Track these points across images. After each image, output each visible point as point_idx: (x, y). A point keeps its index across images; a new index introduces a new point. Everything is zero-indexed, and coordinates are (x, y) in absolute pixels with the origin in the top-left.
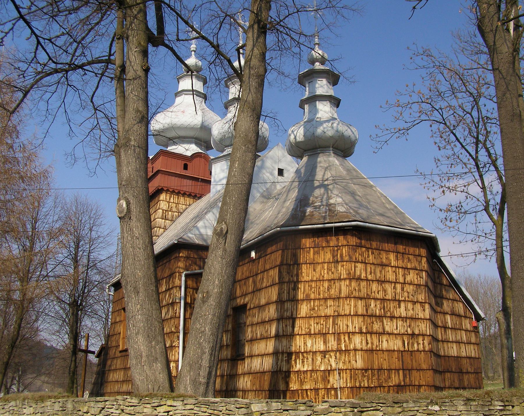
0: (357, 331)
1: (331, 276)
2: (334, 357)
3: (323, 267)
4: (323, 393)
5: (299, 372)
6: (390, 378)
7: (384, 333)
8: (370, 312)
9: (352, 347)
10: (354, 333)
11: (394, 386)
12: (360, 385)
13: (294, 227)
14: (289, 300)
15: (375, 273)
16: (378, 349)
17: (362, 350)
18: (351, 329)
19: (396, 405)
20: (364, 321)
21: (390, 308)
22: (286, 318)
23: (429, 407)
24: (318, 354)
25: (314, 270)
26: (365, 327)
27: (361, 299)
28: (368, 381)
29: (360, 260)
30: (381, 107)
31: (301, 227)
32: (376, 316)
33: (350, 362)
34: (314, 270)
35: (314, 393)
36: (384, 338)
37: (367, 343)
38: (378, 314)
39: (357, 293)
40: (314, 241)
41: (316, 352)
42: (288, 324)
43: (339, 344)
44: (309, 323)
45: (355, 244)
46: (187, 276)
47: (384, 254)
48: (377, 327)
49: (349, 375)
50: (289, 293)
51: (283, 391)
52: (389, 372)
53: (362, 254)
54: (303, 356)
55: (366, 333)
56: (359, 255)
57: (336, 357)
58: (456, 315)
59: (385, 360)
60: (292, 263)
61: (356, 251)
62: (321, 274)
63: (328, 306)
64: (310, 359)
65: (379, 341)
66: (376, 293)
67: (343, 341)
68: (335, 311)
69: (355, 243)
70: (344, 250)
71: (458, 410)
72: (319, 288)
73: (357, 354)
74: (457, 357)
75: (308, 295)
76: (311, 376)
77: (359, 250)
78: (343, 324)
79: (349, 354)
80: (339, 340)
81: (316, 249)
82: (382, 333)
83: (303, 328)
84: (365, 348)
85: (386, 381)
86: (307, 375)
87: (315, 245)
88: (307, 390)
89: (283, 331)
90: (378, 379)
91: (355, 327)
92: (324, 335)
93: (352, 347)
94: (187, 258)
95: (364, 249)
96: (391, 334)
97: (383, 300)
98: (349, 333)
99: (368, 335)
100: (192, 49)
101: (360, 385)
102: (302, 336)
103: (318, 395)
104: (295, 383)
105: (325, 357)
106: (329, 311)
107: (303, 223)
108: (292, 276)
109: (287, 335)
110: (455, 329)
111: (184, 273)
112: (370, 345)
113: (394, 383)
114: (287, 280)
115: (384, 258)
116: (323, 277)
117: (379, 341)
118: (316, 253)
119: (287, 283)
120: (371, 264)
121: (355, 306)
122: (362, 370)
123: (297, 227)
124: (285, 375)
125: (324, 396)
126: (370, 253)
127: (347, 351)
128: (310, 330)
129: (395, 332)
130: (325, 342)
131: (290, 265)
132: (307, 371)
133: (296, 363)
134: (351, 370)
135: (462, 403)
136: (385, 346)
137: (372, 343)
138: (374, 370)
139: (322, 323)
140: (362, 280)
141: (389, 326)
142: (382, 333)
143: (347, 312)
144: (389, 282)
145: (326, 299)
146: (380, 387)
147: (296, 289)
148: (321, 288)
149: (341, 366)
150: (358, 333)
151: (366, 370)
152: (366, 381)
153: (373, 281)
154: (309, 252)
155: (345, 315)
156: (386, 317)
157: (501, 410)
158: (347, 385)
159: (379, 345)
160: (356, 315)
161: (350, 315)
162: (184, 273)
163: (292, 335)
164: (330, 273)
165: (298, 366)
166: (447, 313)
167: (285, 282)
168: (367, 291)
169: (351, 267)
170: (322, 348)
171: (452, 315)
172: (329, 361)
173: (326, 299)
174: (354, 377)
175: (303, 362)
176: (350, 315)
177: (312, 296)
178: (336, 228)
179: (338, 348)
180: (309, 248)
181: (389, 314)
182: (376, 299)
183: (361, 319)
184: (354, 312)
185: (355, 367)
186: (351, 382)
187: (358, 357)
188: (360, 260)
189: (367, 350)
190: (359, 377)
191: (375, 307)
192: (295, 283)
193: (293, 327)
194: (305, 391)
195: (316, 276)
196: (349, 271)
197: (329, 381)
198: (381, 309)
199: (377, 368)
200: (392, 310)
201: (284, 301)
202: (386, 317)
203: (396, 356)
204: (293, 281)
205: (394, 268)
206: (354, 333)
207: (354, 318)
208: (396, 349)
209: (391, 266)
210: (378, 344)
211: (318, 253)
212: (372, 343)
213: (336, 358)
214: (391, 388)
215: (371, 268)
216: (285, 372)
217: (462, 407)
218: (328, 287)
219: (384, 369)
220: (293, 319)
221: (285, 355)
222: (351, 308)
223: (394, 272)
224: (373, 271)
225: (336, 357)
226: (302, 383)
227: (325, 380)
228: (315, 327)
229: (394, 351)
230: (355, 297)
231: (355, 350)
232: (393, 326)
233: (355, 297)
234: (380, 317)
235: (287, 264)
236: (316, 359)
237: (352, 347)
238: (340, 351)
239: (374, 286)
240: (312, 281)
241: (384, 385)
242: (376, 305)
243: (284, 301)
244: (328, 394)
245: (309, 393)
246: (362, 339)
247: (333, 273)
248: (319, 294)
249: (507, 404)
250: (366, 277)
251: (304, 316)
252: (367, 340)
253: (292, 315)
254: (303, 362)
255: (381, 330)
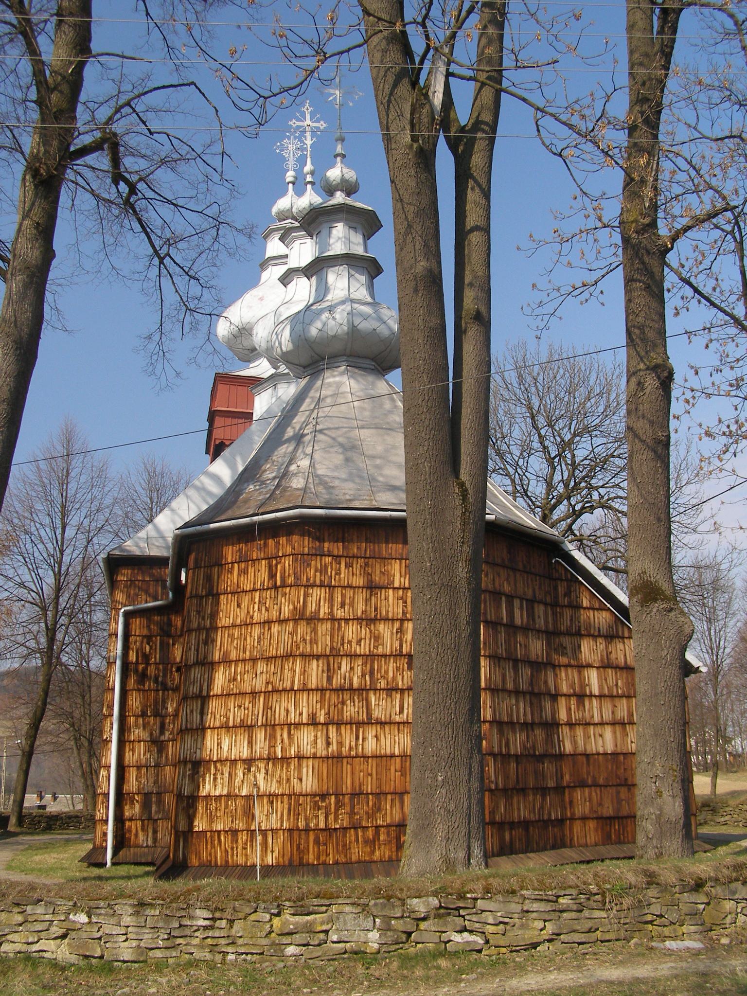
0: (305, 721)
1: (265, 616)
2: (263, 771)
3: (253, 599)
4: (244, 838)
5: (208, 797)
6: (379, 809)
7: (369, 722)
8: (336, 682)
9: (293, 752)
10: (298, 725)
11: (388, 826)
12: (307, 825)
13: (198, 528)
14: (198, 663)
15: (352, 604)
16: (353, 753)
17: (314, 757)
18: (293, 718)
19: (16, 910)
20: (322, 701)
21: (387, 672)
22: (192, 697)
23: (71, 916)
24: (239, 764)
25: (239, 606)
26: (323, 712)
27: (318, 657)
28: (326, 818)
29: (318, 582)
30: (518, 249)
31: (212, 526)
32: (351, 689)
33: (288, 780)
34: (239, 606)
35: (230, 837)
36: (371, 732)
37: (328, 744)
38: (356, 685)
39: (308, 646)
40: (240, 550)
41: (235, 760)
42: (195, 708)
43: (272, 746)
44: (226, 705)
45: (306, 550)
46: (127, 615)
47: (378, 566)
48: (351, 710)
49: (286, 806)
50: (198, 651)
51: (183, 832)
52: (379, 800)
53: (323, 570)
54: (216, 767)
55: (326, 724)
56: (316, 571)
57: (267, 771)
58: (617, 668)
59: (371, 775)
60: (204, 593)
61: (309, 565)
62: (248, 612)
63: (258, 673)
64: (227, 775)
65: (357, 738)
66: (354, 644)
67: (279, 741)
68: (267, 683)
69: (306, 549)
70: (287, 562)
71: (122, 924)
72: (245, 639)
73: (304, 764)
74: (615, 754)
75: (226, 654)
76: (227, 806)
77: (316, 563)
78: (285, 708)
79: (289, 764)
80: (273, 737)
81: (243, 565)
82: (363, 723)
83: (218, 716)
84: (321, 751)
85: (370, 816)
86: (221, 803)
87: (240, 557)
88: (219, 832)
89: (187, 721)
90: (352, 813)
91: (301, 714)
92: (248, 728)
93: (293, 752)
94: (132, 582)
95: (328, 560)
96: (386, 723)
97: (370, 657)
98: (290, 725)
99: (330, 727)
100: (288, 180)
101: (307, 825)
102: (216, 730)
103: (237, 841)
104: (202, 818)
105: (249, 770)
106: (259, 684)
107: (229, 513)
108: (203, 619)
109: (192, 729)
110: (611, 697)
111: (122, 610)
112: (334, 747)
113: (389, 820)
114: (195, 625)
115: (378, 572)
116: (252, 617)
117: (357, 738)
118: (244, 572)
119: (196, 630)
120: (344, 587)
121: (304, 672)
122: (314, 795)
123: (205, 527)
124: (188, 803)
125: (246, 844)
126: (343, 566)
127: (285, 759)
128: (228, 719)
129: (397, 719)
130: (250, 743)
131: (202, 597)
132: (221, 796)
133: (204, 780)
134: (290, 796)
135: (130, 911)
136: (371, 746)
137: (340, 744)
138: (343, 795)
139: (246, 705)
140: (319, 620)
141: (380, 707)
142: (363, 723)
143: (288, 685)
144: (386, 619)
145: (254, 660)
146: (355, 828)
147: (209, 641)
148: (248, 638)
149: (274, 788)
150: (308, 724)
151: (324, 796)
152: (322, 818)
153: (347, 620)
154: (231, 571)
155: (284, 690)
156: (375, 690)
157: (206, 928)
158: (282, 825)
159: (356, 745)
160: (305, 689)
161: (292, 689)
162: (122, 610)
163: (201, 730)
164: (264, 609)
165: (207, 788)
166: (589, 666)
167: (192, 630)
168: (332, 641)
169: (299, 597)
170: (245, 754)
171: (604, 667)
172: (255, 777)
173: (254, 660)
174: (294, 811)
175: (215, 779)
176: (292, 689)
177: (233, 655)
178: (262, 524)
179: (269, 753)
180: (232, 563)
181: (383, 684)
182: (353, 656)
183: (315, 697)
184: (299, 684)
185: (297, 790)
186: (289, 819)
187: (305, 770)
188: (318, 582)
189: (328, 758)
190: (306, 810)
191: (349, 672)
192: (208, 630)
193: (202, 713)
194: (216, 834)
195: (242, 615)
196: (294, 605)
197: (253, 816)
198: (363, 675)
199: (349, 791)
200: (391, 674)
201: (191, 666)
202: (375, 690)
203: (398, 766)
204: (205, 628)
205: (401, 592)
206: (298, 725)
207: (299, 695)
208: (397, 753)
209: (394, 588)
210: (353, 744)
211: (245, 572)
212: (340, 744)
213: (267, 773)
214: (382, 829)
215: (343, 596)
216: (188, 797)
217: (129, 919)
218: (259, 638)
219: (367, 794)
220: (204, 699)
221: (189, 766)
222: (294, 677)
223: (402, 598)
224: (347, 601)
225: (267, 771)
226: (211, 819)
227: (249, 815)
228: (235, 715)
229: (392, 756)
230: (303, 656)
231: (300, 757)
232: (393, 706)
233: (303, 656)
234: (362, 691)
235: (196, 596)
236: (236, 774)
237: (293, 752)
238: (271, 759)
239: (351, 631)
240: (234, 626)
241: (364, 824)
242: (352, 669)
243: (191, 666)
244: (252, 841)
245: (222, 838)
246: (316, 736)
247: (267, 610)
248: (244, 652)
249: (218, 915)
250: (331, 613)
251: (219, 693)
252: (328, 737)
253: (201, 691)
254: (215, 779)
255: (363, 717)
